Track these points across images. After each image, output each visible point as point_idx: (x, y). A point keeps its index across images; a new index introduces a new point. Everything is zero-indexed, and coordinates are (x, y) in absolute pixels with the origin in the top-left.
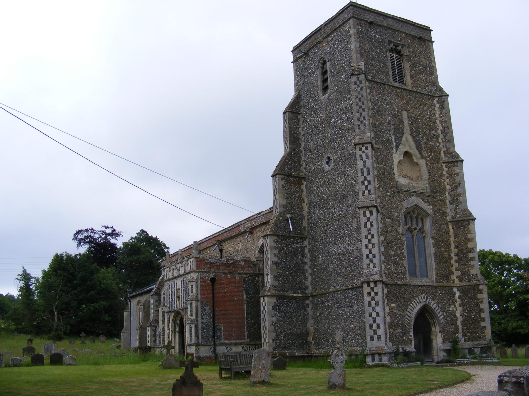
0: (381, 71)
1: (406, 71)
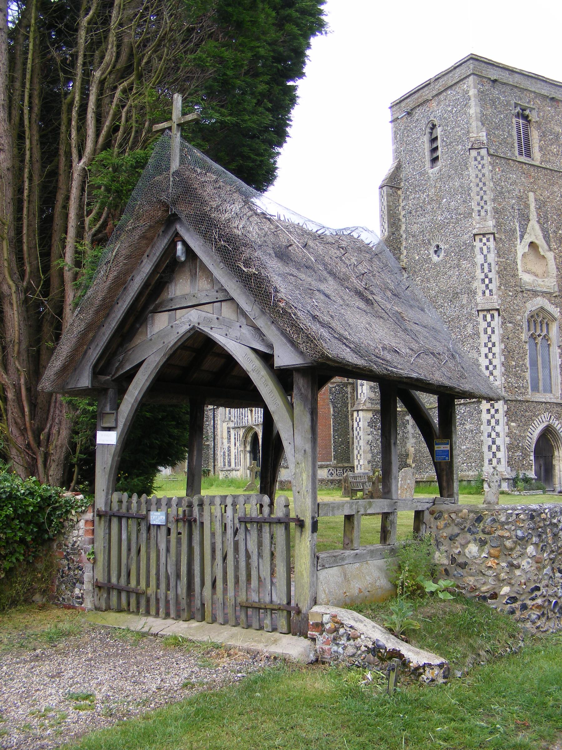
0: (505, 142)
1: (534, 141)
